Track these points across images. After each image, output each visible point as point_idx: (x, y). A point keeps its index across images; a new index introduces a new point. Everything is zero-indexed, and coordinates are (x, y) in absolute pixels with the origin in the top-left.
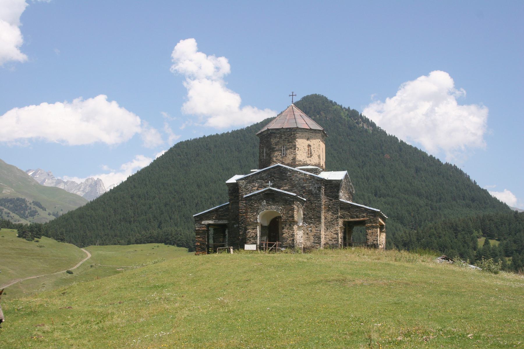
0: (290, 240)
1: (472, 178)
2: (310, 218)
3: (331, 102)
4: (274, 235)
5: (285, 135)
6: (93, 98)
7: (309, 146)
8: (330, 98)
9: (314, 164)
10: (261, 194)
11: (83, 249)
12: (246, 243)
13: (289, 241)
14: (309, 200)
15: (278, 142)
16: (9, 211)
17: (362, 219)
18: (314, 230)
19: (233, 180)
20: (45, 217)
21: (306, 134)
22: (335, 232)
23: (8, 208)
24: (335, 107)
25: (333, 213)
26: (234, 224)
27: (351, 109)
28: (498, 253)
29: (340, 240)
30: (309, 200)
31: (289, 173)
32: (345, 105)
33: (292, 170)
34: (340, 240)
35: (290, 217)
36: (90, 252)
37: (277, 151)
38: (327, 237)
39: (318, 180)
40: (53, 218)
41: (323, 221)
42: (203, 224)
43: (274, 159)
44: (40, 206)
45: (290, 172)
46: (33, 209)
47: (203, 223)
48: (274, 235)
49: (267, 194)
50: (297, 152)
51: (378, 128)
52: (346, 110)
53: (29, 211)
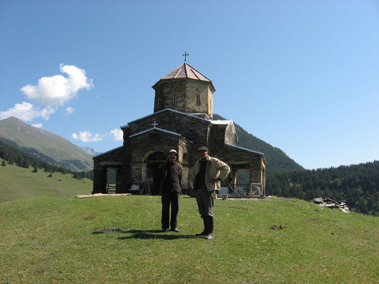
1: (287, 154)
5: (176, 85)
6: (48, 77)
10: (146, 135)
15: (170, 91)
16: (73, 166)
31: (177, 117)
39: (205, 124)
42: (101, 165)
44: (87, 164)
45: (179, 116)
46: (84, 165)
49: (152, 134)
51: (244, 130)
53: (82, 166)
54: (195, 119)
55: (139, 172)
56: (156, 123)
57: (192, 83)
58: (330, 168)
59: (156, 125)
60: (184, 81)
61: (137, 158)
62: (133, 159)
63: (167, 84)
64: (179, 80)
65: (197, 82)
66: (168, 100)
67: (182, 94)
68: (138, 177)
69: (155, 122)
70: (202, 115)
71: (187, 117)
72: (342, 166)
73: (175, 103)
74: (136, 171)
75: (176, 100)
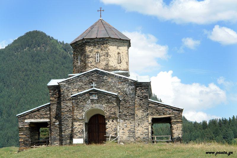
0: (113, 134)
2: (126, 116)
3: (49, 37)
7: (119, 53)
8: (48, 34)
9: (123, 69)
14: (124, 100)
18: (128, 126)
19: (54, 82)
21: (116, 43)
22: (146, 127)
24: (52, 41)
27: (65, 43)
30: (124, 100)
32: (60, 40)
33: (108, 73)
37: (91, 57)
42: (26, 123)
43: (89, 65)
50: (109, 59)
52: (61, 44)
54: (122, 78)
55: (81, 128)
56: (95, 84)
57: (113, 42)
58: (231, 118)
59: (95, 86)
60: (106, 41)
61: (79, 115)
62: (75, 116)
63: (89, 43)
64: (101, 40)
65: (117, 40)
66: (91, 58)
67: (104, 52)
68: (81, 131)
69: (94, 83)
70: (125, 73)
71: (114, 76)
72: (210, 121)
73: (98, 62)
74: (78, 127)
75: (98, 58)
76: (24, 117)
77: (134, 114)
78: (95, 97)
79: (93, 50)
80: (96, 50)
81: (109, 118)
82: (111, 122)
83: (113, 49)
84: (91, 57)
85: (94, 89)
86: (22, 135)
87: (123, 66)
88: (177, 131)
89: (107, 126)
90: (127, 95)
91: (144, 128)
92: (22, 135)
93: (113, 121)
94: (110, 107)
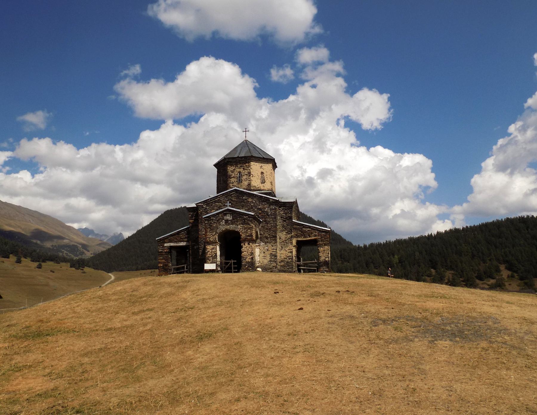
2: (267, 238)
4: (234, 260)
7: (262, 173)
11: (109, 274)
12: (206, 262)
13: (248, 259)
14: (265, 221)
17: (313, 238)
18: (270, 249)
20: (88, 255)
23: (66, 250)
25: (287, 233)
26: (194, 245)
28: (395, 265)
29: (294, 258)
34: (294, 258)
35: (248, 236)
36: (114, 276)
37: (233, 177)
38: (282, 255)
40: (92, 255)
41: (278, 240)
43: (231, 185)
47: (166, 245)
48: (234, 260)
50: (252, 178)
76: (163, 241)
77: (276, 237)
78: (229, 217)
79: (234, 170)
80: (238, 170)
81: (245, 240)
82: (246, 244)
83: (255, 167)
84: (233, 177)
85: (228, 209)
86: (161, 259)
87: (267, 186)
88: (325, 253)
89: (243, 249)
90: (268, 215)
91: (287, 251)
92: (161, 259)
93: (249, 244)
94: (245, 228)
